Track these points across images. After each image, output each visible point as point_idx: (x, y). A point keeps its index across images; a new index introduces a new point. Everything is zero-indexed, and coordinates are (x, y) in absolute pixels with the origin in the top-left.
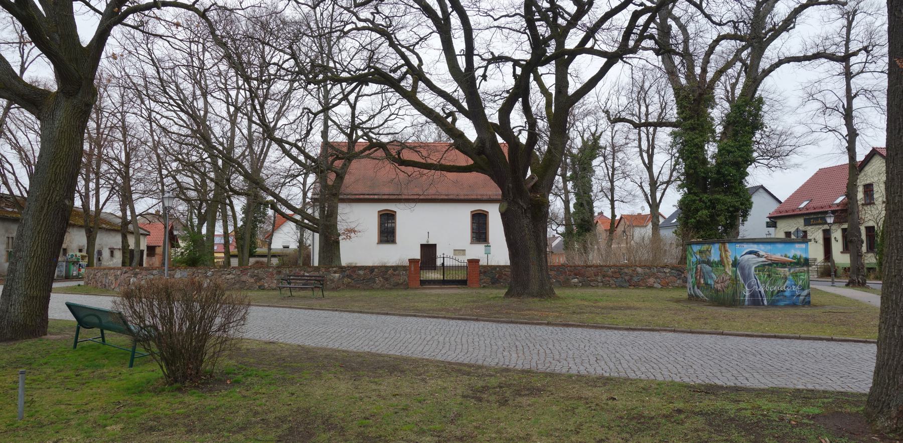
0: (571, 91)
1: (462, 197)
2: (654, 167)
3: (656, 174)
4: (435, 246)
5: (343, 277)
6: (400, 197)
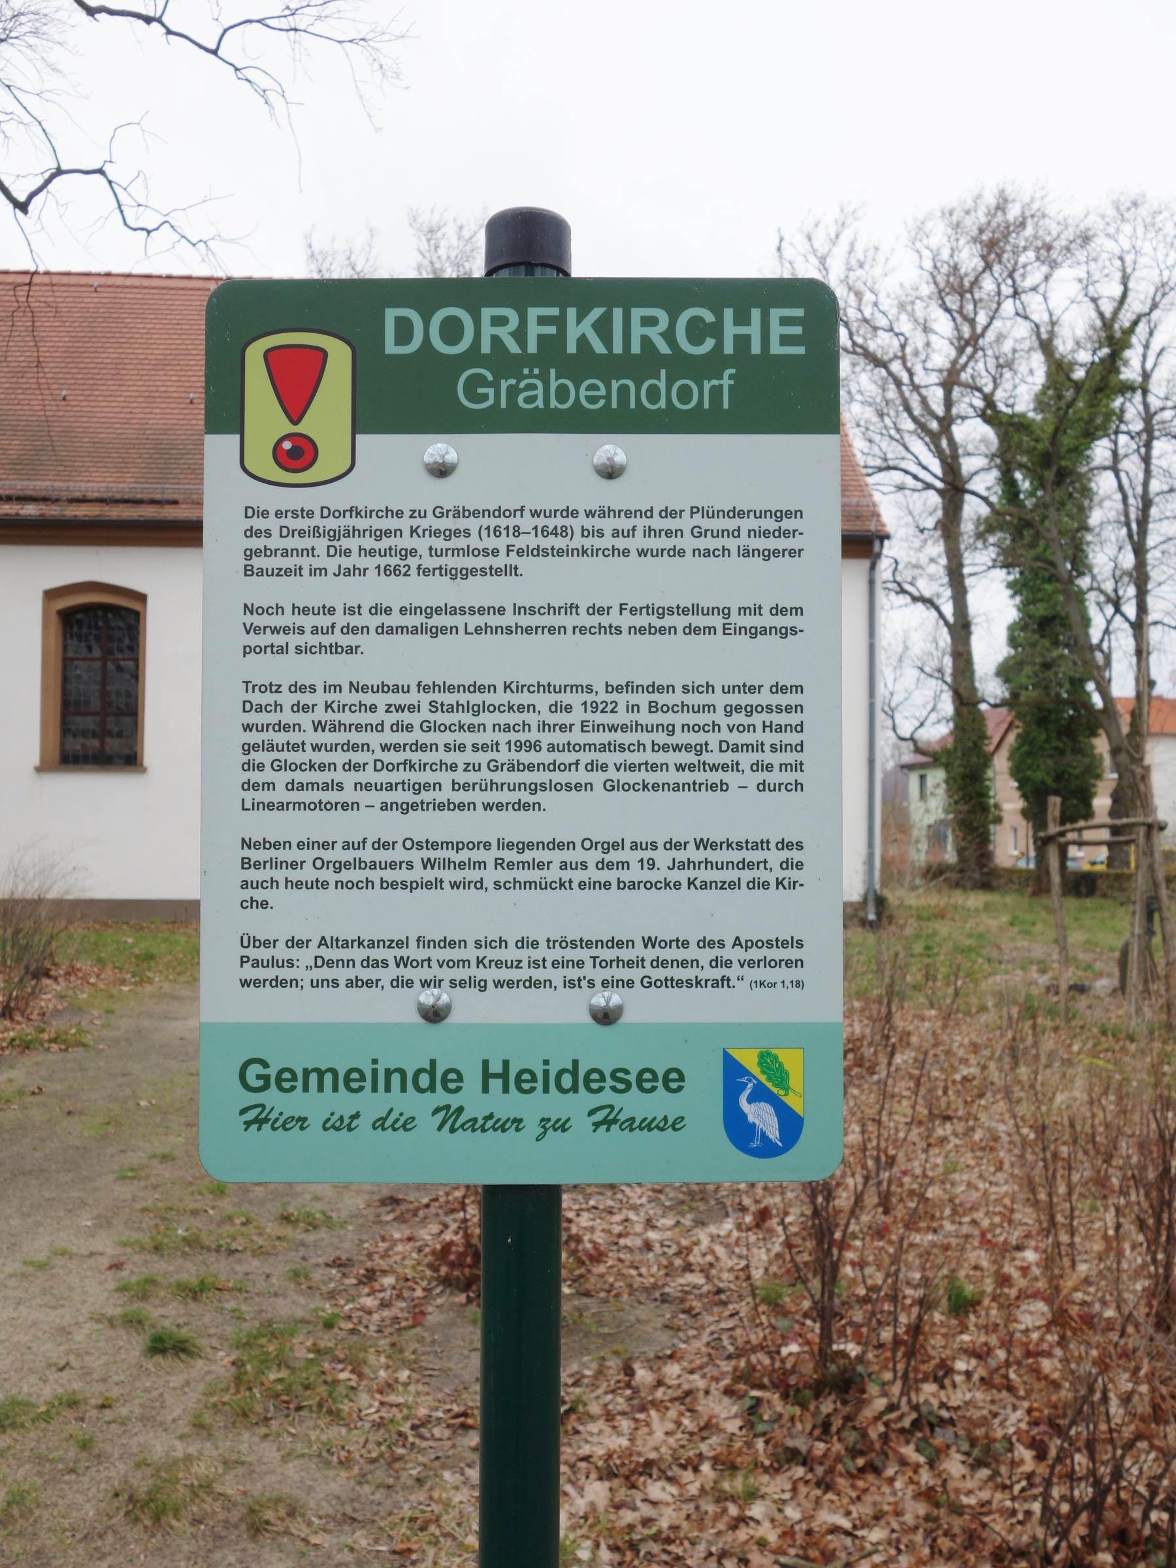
6: (169, 513)
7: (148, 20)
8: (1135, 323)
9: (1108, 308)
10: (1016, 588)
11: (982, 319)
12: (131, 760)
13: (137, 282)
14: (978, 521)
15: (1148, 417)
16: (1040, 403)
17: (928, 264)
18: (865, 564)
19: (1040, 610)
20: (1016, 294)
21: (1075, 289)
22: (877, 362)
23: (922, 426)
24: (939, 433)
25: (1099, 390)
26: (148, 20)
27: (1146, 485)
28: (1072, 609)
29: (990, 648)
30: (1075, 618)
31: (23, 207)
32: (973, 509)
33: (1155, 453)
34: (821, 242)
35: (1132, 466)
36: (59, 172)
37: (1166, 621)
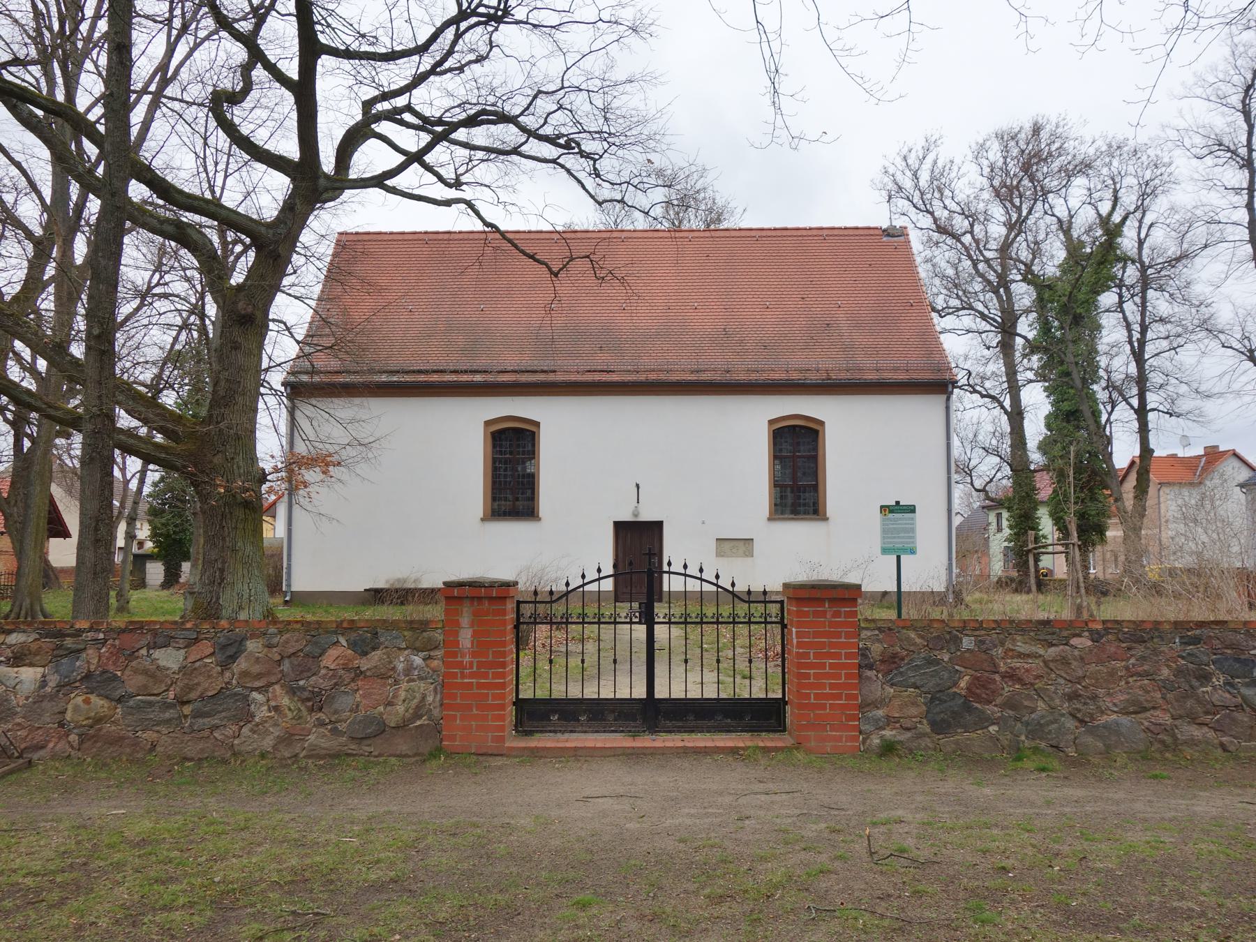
0: (388, 182)
1: (742, 377)
5: (66, 686)
6: (551, 377)
10: (1050, 391)
12: (662, 522)
17: (986, 170)
18: (944, 397)
19: (1066, 406)
29: (1035, 430)
31: (556, 275)
36: (572, 259)
37: (1161, 408)
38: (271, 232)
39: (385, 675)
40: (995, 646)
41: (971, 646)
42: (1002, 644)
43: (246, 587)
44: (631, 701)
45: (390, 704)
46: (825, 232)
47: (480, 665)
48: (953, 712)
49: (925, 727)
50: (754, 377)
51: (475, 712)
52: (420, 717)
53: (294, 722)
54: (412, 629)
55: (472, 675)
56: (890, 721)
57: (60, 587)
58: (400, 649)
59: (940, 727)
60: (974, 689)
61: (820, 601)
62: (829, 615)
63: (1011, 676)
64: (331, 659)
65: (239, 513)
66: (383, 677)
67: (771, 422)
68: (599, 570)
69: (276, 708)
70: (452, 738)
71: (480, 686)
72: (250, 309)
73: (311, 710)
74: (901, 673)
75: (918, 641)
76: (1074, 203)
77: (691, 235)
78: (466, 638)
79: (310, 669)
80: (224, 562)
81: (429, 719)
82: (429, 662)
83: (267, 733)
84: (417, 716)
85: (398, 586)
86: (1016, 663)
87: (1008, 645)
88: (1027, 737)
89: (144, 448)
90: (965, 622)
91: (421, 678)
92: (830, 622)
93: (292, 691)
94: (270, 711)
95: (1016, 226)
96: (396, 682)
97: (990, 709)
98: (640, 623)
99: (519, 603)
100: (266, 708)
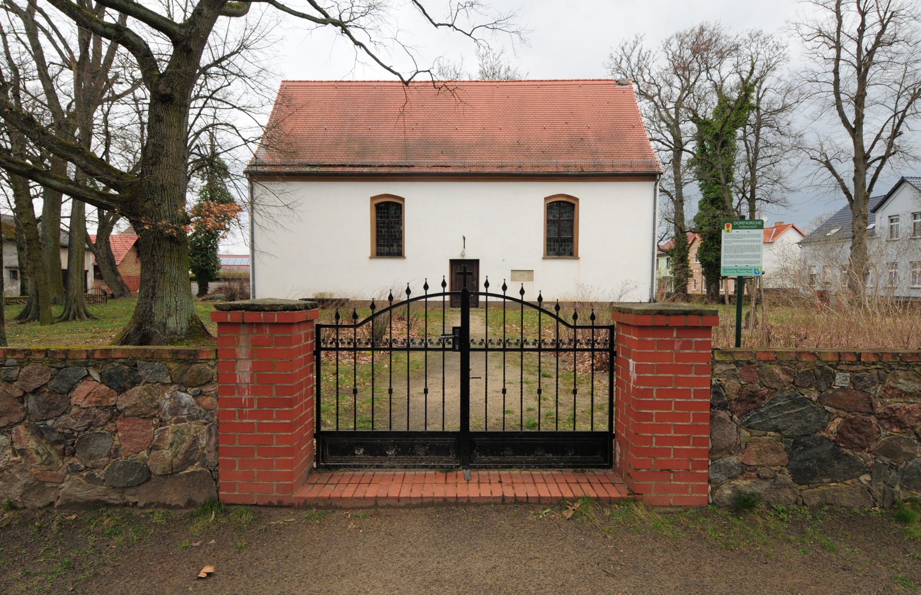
1: (529, 170)
2: (865, 128)
3: (867, 144)
4: (476, 262)
7: (450, 26)
8: (756, 82)
9: (745, 77)
10: (702, 187)
11: (692, 80)
13: (388, 84)
14: (688, 161)
15: (759, 117)
16: (716, 113)
19: (712, 195)
20: (707, 69)
21: (731, 68)
22: (651, 98)
23: (668, 125)
24: (674, 127)
25: (740, 109)
26: (450, 26)
27: (756, 144)
28: (726, 195)
29: (691, 210)
30: (727, 199)
32: (685, 157)
33: (761, 132)
34: (628, 50)
35: (752, 138)
36: (418, 72)
38: (183, 31)
39: (149, 414)
40: (873, 383)
41: (846, 384)
42: (882, 380)
43: (173, 300)
44: (443, 434)
45: (153, 448)
46: (581, 83)
47: (261, 403)
48: (819, 460)
49: (786, 477)
50: (536, 170)
51: (256, 457)
52: (192, 463)
53: (44, 468)
54: (177, 360)
55: (252, 415)
56: (744, 469)
57: (131, 296)
58: (164, 384)
59: (802, 476)
60: (846, 433)
61: (667, 328)
62: (676, 346)
63: (891, 418)
64: (82, 395)
65: (166, 245)
66: (146, 417)
67: (546, 199)
68: (426, 287)
69: (22, 452)
70: (232, 487)
71: (262, 427)
72: (168, 91)
73: (63, 454)
74: (761, 414)
75: (783, 377)
76: (724, 73)
77: (498, 84)
78: (244, 371)
79: (58, 407)
80: (155, 282)
81: (203, 465)
82: (200, 399)
83: (14, 479)
84: (188, 461)
85: (320, 297)
86: (896, 403)
87: (889, 382)
88: (902, 487)
89: (93, 196)
90: (839, 354)
91: (191, 418)
92: (678, 355)
93: (40, 433)
94: (15, 454)
95: (687, 89)
96: (162, 422)
97: (864, 457)
98: (453, 349)
99: (319, 327)
100: (10, 451)
